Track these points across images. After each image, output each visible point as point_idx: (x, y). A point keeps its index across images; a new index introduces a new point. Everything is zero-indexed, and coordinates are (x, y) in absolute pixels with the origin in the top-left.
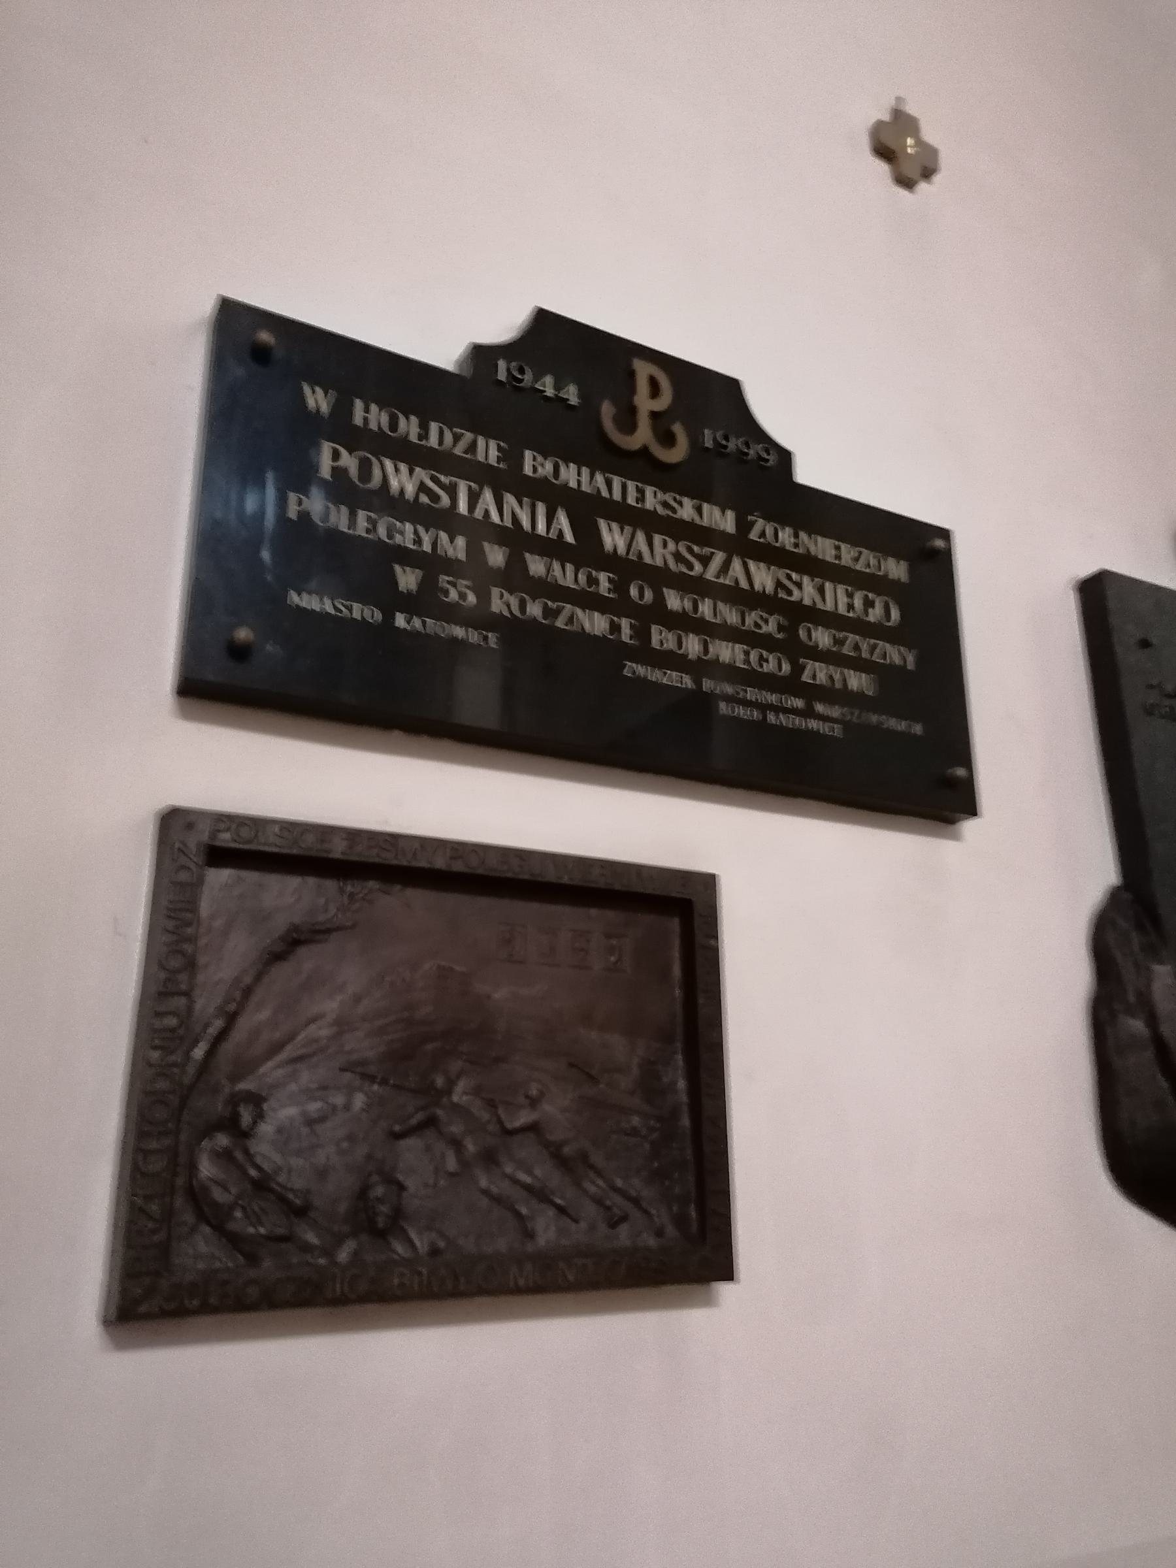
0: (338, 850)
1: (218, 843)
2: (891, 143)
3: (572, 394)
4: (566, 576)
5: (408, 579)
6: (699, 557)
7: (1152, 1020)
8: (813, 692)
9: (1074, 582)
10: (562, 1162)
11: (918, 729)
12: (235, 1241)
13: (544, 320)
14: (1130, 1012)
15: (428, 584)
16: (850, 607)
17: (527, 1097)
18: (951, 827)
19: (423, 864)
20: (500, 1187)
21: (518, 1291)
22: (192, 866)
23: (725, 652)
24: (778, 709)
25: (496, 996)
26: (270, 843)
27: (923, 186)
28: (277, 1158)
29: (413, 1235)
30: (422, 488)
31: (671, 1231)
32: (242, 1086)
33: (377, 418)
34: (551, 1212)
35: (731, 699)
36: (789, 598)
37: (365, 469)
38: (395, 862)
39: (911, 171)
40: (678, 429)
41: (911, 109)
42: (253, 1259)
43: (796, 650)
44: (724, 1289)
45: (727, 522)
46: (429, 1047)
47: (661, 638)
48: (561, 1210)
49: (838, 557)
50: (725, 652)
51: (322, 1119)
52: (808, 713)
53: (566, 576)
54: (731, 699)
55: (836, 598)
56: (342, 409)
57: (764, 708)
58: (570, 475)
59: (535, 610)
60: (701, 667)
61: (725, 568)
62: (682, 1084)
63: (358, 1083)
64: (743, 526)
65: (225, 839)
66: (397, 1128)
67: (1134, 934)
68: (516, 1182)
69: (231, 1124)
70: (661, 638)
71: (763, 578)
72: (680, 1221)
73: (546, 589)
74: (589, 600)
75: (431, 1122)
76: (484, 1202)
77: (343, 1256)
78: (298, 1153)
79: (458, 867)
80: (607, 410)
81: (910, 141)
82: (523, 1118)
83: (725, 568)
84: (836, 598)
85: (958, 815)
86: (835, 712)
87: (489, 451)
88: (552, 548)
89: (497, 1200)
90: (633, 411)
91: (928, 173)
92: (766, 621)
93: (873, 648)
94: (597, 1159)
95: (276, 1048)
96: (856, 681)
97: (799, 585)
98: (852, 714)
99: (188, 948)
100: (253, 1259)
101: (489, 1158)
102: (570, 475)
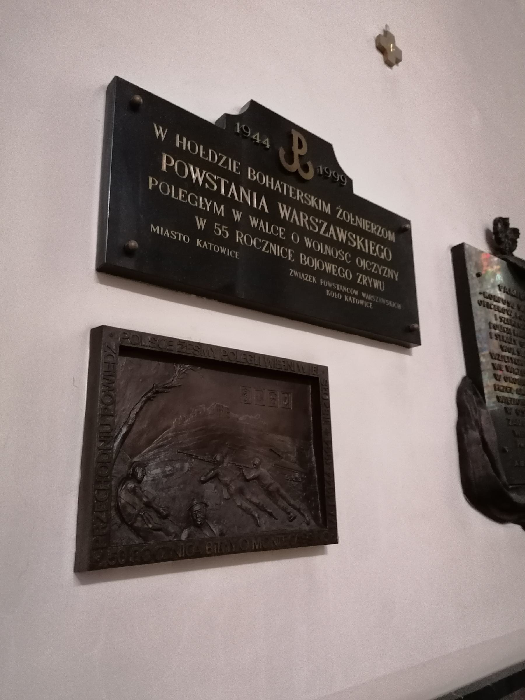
0: (176, 350)
1: (123, 344)
2: (384, 45)
3: (267, 142)
4: (265, 227)
5: (201, 224)
6: (318, 224)
7: (481, 432)
8: (362, 288)
9: (451, 248)
10: (269, 493)
11: (399, 307)
12: (137, 531)
13: (253, 105)
14: (473, 428)
15: (209, 226)
16: (374, 251)
17: (254, 464)
18: (408, 349)
19: (211, 358)
20: (246, 505)
21: (256, 550)
22: (113, 355)
23: (329, 267)
24: (349, 295)
25: (240, 419)
26: (147, 345)
27: (395, 67)
28: (153, 492)
29: (211, 526)
30: (205, 180)
31: (313, 523)
32: (136, 459)
33: (186, 145)
34: (266, 516)
35: (331, 289)
36: (317, 242)
37: (181, 167)
38: (200, 356)
39: (392, 60)
40: (309, 164)
41: (392, 31)
42: (145, 539)
43: (355, 269)
44: (330, 547)
45: (328, 209)
46: (214, 441)
47: (304, 260)
48: (271, 514)
49: (370, 228)
50: (329, 267)
51: (172, 475)
52: (359, 297)
53: (265, 227)
54: (331, 289)
55: (370, 247)
56: (170, 137)
57: (343, 294)
58: (266, 180)
59: (253, 242)
60: (320, 274)
61: (327, 230)
62: (314, 459)
63: (185, 458)
64: (334, 211)
65: (128, 343)
66: (202, 478)
67: (474, 397)
68: (251, 502)
69: (133, 476)
70: (304, 260)
71: (342, 235)
72: (315, 518)
73: (256, 232)
74: (275, 240)
75: (216, 476)
76: (240, 511)
77: (184, 536)
78: (163, 490)
79: (225, 360)
80: (282, 152)
81: (391, 46)
82: (252, 474)
83: (327, 230)
84: (370, 247)
85: (412, 344)
86: (369, 297)
87: (233, 166)
88: (259, 214)
89: (245, 510)
90: (292, 153)
91: (398, 61)
92: (339, 255)
93: (383, 270)
94: (283, 491)
95: (150, 441)
96: (377, 284)
97: (356, 240)
98: (376, 299)
99: (112, 393)
100: (145, 539)
101: (241, 491)
102: (266, 180)
